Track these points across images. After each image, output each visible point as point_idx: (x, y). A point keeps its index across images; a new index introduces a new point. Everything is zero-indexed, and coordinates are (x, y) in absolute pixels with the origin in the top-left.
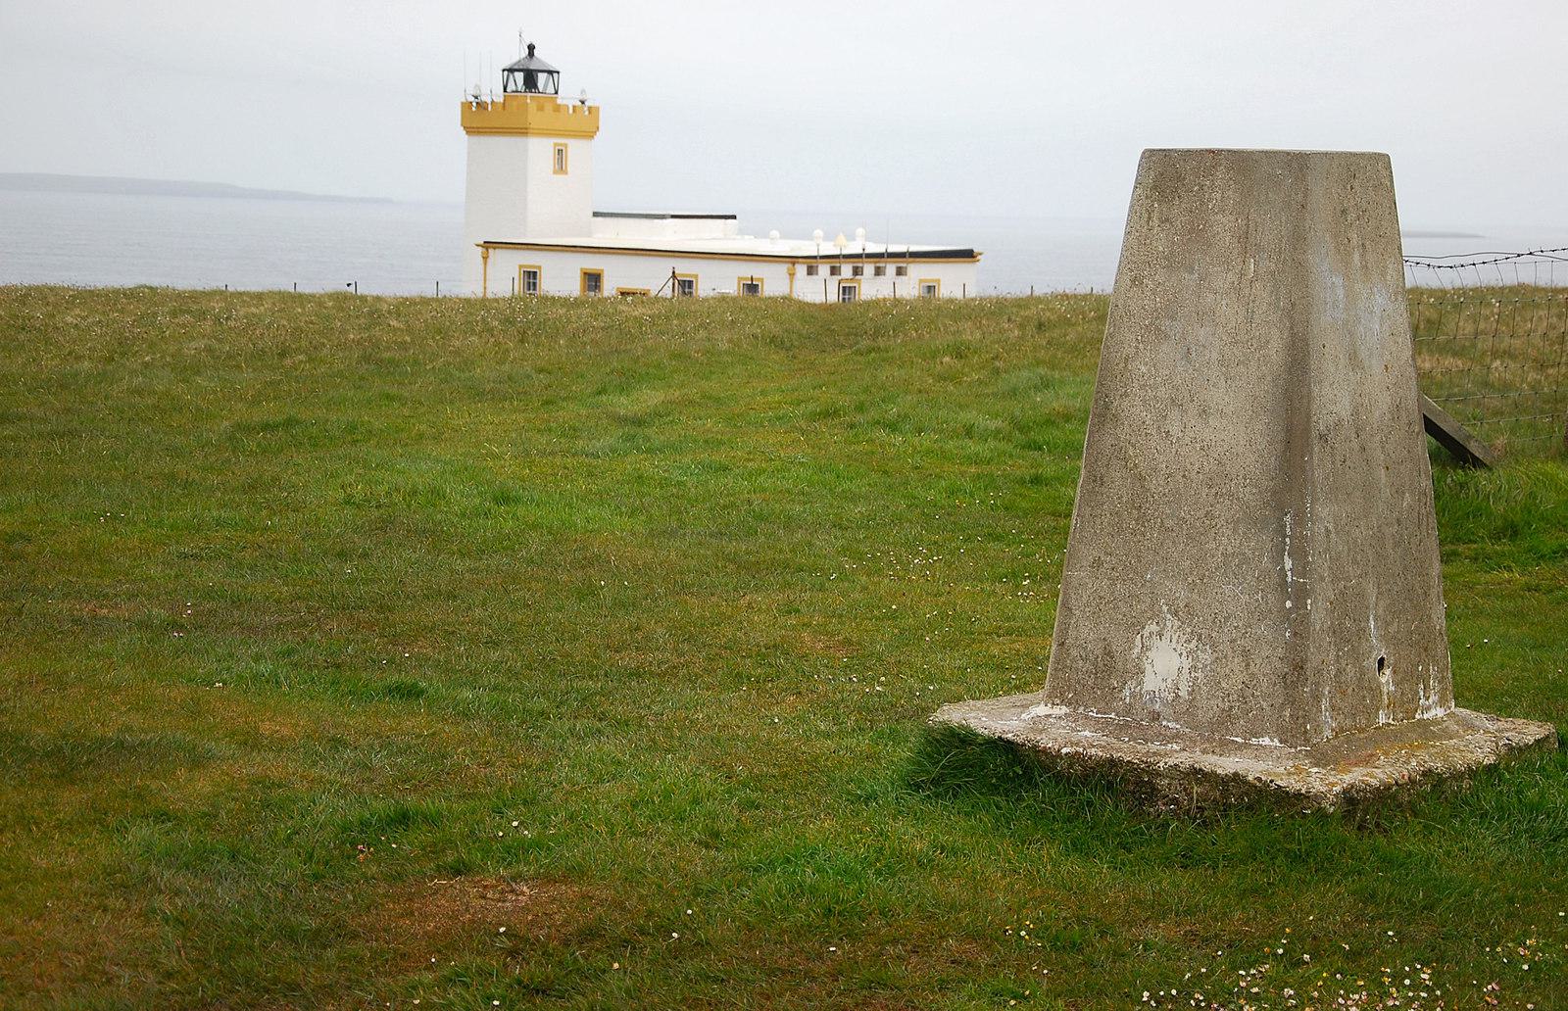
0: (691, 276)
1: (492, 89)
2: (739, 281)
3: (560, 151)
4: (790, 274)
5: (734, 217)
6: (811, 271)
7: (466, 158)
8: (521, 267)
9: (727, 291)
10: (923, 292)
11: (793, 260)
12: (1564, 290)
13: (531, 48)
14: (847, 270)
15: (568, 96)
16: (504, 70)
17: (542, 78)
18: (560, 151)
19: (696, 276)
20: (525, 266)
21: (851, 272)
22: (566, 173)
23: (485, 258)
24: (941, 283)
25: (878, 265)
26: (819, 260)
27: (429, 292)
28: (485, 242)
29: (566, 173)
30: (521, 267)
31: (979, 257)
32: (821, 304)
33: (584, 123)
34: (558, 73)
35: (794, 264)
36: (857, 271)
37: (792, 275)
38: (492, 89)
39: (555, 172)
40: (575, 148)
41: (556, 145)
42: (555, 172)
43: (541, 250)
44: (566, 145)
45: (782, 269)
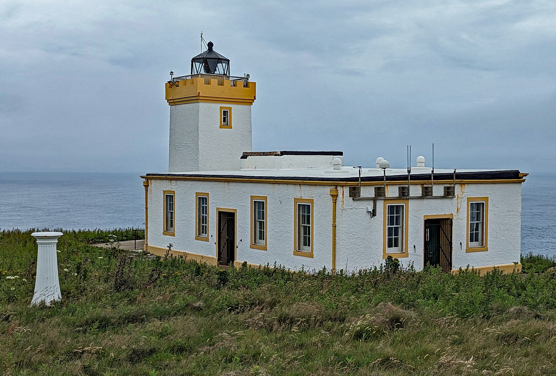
4: (333, 196)
5: (341, 154)
6: (354, 193)
7: (200, 124)
9: (131, 227)
10: (205, 49)
11: (335, 183)
13: (210, 45)
14: (392, 191)
15: (235, 72)
16: (194, 60)
18: (225, 113)
23: (147, 186)
25: (425, 186)
26: (385, 182)
28: (147, 175)
33: (246, 91)
34: (229, 61)
35: (336, 186)
36: (404, 194)
37: (335, 197)
38: (184, 70)
40: (237, 111)
43: (315, 185)
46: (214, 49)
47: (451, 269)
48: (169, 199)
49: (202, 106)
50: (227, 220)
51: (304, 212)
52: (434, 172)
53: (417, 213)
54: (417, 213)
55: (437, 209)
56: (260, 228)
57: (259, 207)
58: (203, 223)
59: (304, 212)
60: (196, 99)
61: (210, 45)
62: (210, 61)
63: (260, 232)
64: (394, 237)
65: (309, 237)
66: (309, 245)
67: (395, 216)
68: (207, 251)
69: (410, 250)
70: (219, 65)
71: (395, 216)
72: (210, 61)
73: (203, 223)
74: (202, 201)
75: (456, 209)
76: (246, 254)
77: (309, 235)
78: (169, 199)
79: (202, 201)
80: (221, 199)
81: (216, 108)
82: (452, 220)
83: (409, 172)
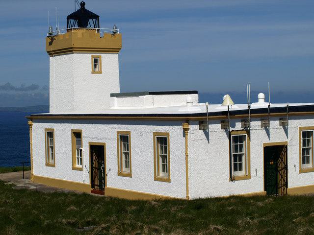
3: (96, 61)
8: (300, 129)
13: (83, 4)
16: (69, 17)
18: (96, 61)
19: (129, 133)
22: (101, 73)
30: (300, 129)
34: (98, 17)
39: (93, 72)
42: (93, 72)
44: (100, 57)
47: (287, 188)
48: (50, 135)
49: (76, 56)
50: (98, 151)
51: (162, 141)
52: (271, 107)
53: (259, 139)
54: (259, 139)
56: (126, 158)
57: (124, 139)
58: (78, 156)
59: (162, 141)
60: (69, 50)
63: (126, 162)
64: (237, 162)
65: (167, 165)
66: (167, 172)
67: (238, 143)
68: (83, 178)
69: (253, 173)
70: (91, 20)
71: (238, 143)
73: (78, 156)
74: (77, 135)
76: (114, 182)
77: (167, 163)
78: (50, 135)
79: (77, 135)
80: (92, 133)
81: (86, 59)
82: (287, 146)
83: (249, 107)
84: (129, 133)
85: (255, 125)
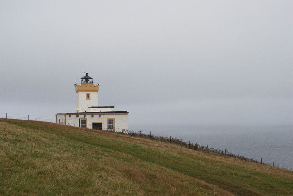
0: (108, 120)
1: (79, 83)
2: (80, 119)
3: (88, 95)
5: (114, 107)
6: (70, 116)
8: (108, 118)
10: (85, 75)
12: (291, 172)
13: (87, 74)
15: (95, 83)
16: (81, 79)
17: (90, 80)
18: (88, 95)
19: (114, 118)
20: (109, 118)
21: (83, 117)
22: (90, 99)
24: (115, 119)
27: (27, 119)
29: (90, 99)
30: (108, 118)
31: (128, 113)
32: (64, 125)
40: (93, 95)
41: (87, 93)
44: (90, 94)
45: (63, 117)
46: (88, 75)
55: (96, 119)
61: (87, 74)
62: (87, 78)
72: (87, 78)
75: (104, 121)
84: (114, 118)
85: (88, 116)
